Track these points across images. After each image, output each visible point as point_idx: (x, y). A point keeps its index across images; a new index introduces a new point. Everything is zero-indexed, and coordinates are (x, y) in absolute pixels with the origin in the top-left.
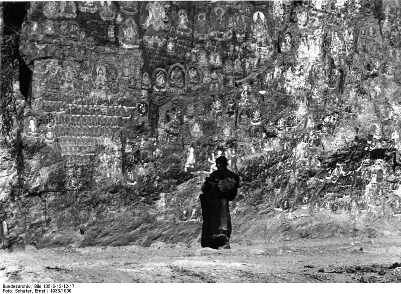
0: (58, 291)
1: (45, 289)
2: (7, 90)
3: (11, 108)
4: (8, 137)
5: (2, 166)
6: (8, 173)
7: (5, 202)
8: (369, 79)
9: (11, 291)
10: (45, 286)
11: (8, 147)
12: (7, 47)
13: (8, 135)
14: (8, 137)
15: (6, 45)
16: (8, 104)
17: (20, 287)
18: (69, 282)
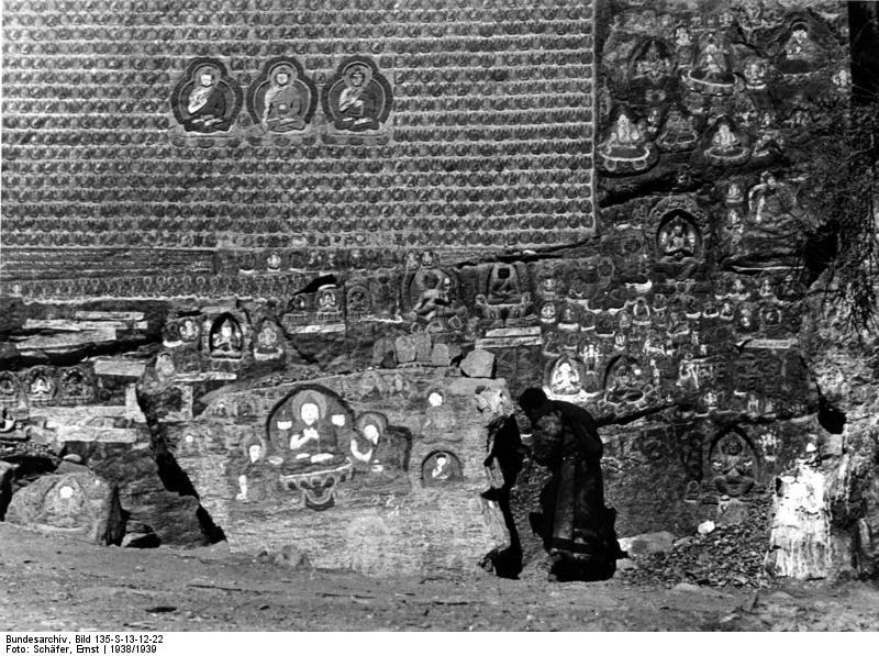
0: (127, 649)
1: (100, 645)
2: (861, 229)
3: (871, 266)
4: (865, 333)
5: (853, 395)
6: (866, 411)
7: (862, 477)
8: (348, 223)
9: (23, 650)
10: (100, 639)
11: (865, 355)
12: (861, 133)
13: (866, 327)
14: (865, 333)
15: (859, 129)
16: (865, 257)
17: (43, 640)
18: (113, 630)
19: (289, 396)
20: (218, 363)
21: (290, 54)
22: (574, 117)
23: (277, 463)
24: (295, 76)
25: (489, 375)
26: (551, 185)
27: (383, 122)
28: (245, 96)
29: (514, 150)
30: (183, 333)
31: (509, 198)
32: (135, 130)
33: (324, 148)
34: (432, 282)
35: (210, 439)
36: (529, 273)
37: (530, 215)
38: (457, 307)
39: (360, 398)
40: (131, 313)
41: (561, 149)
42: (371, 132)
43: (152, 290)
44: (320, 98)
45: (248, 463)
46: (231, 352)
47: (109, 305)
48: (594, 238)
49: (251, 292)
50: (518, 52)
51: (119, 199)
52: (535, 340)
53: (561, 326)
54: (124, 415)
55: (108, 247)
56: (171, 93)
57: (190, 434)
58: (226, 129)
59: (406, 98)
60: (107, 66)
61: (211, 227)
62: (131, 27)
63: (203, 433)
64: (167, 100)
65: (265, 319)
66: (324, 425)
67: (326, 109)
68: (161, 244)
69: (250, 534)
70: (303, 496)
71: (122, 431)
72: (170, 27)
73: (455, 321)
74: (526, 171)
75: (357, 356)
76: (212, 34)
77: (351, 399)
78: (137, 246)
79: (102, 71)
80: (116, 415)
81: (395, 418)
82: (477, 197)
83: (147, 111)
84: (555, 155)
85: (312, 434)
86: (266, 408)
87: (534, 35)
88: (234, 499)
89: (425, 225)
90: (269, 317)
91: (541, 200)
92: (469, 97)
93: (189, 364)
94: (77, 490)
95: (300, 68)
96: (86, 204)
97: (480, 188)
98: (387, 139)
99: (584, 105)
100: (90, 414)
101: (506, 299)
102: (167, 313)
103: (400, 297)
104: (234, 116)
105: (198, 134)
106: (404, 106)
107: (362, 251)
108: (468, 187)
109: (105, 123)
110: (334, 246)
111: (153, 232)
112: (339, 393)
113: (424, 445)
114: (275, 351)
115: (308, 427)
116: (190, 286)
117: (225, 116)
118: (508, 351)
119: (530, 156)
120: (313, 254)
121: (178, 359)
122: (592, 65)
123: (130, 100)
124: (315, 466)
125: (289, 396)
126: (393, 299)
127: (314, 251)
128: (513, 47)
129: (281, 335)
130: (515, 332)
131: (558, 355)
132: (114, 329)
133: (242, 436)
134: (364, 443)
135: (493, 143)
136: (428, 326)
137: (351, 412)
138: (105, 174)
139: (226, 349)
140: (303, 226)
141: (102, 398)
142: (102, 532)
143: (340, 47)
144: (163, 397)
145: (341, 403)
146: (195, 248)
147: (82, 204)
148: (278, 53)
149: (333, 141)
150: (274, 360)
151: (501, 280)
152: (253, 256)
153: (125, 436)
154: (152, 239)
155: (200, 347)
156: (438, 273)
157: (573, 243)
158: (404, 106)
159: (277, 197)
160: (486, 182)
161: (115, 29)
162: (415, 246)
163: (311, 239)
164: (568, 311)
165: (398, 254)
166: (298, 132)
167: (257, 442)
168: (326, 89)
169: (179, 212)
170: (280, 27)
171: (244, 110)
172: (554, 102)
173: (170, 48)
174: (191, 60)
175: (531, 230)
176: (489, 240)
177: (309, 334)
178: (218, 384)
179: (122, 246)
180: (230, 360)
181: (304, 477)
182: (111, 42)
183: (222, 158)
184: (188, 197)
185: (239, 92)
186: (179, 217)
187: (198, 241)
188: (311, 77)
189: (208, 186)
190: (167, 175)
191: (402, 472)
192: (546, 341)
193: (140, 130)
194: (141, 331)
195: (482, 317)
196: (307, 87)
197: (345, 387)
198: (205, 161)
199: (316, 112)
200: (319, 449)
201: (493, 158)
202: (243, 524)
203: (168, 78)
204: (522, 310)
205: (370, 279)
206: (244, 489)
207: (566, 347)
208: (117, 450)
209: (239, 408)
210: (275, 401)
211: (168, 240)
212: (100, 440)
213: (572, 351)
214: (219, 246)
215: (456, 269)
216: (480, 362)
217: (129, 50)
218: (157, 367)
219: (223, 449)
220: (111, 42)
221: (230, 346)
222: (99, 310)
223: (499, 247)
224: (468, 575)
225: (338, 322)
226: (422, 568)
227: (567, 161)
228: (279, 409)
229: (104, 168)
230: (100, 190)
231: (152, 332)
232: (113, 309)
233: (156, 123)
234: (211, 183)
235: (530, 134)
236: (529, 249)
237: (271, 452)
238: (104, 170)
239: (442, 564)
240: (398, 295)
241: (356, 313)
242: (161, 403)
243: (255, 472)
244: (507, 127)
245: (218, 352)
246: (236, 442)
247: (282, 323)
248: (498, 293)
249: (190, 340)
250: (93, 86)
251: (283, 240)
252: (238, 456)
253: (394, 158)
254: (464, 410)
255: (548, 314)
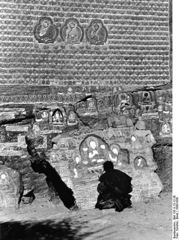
19: (85, 139)
20: (55, 127)
21: (74, 17)
22: (164, 44)
23: (86, 163)
24: (76, 25)
25: (144, 129)
26: (157, 66)
27: (105, 42)
28: (59, 32)
29: (146, 54)
30: (42, 116)
31: (145, 69)
32: (21, 42)
33: (87, 50)
34: (123, 97)
35: (61, 156)
36: (155, 95)
37: (151, 75)
38: (132, 106)
39: (109, 139)
40: (20, 109)
41: (160, 54)
42: (101, 45)
43: (28, 100)
44: (85, 33)
45: (76, 164)
46: (60, 123)
47: (12, 106)
48: (170, 83)
49: (62, 101)
50: (146, 21)
51: (16, 67)
52: (157, 117)
53: (164, 112)
54: (17, 146)
55: (12, 84)
56: (33, 29)
57: (53, 154)
58: (53, 43)
59: (112, 35)
60: (10, 18)
61: (48, 77)
62: (18, 4)
63: (58, 154)
64: (32, 31)
65: (70, 110)
66: (98, 148)
67: (87, 38)
68: (31, 84)
69: (81, 190)
70: (97, 175)
71: (17, 151)
72: (32, 5)
73: (132, 111)
74: (150, 61)
75: (102, 123)
76: (48, 8)
77: (106, 139)
78: (22, 84)
79: (8, 19)
80: (14, 146)
81: (123, 146)
82: (134, 69)
83: (25, 35)
84: (158, 56)
85: (96, 152)
86: (78, 143)
87: (151, 16)
88: (73, 177)
89: (119, 78)
90: (72, 110)
91: (154, 70)
92: (132, 35)
93: (45, 127)
94: (7, 175)
95: (78, 23)
96: (4, 69)
97: (136, 66)
98: (106, 49)
99: (167, 40)
100: (5, 146)
101: (148, 103)
102: (33, 108)
103: (114, 103)
104: (55, 38)
105: (43, 44)
106: (112, 37)
107: (99, 87)
108: (132, 65)
109: (10, 39)
110: (90, 85)
111: (28, 79)
112: (102, 137)
113: (133, 155)
114: (75, 122)
115: (94, 150)
116: (41, 99)
117: (53, 38)
118: (149, 120)
119: (151, 56)
120: (83, 87)
121: (41, 125)
122: (168, 27)
123: (19, 31)
124: (99, 164)
125: (85, 139)
126: (112, 103)
127: (83, 86)
128: (145, 19)
129: (76, 116)
130: (150, 114)
131: (163, 122)
132: (14, 115)
133: (72, 154)
134: (114, 155)
135: (140, 51)
136: (124, 113)
137: (107, 144)
138: (10, 58)
139: (57, 121)
140: (80, 78)
141: (8, 140)
142: (19, 191)
143: (91, 16)
144: (36, 140)
145: (103, 141)
146: (42, 85)
147: (2, 68)
148: (70, 17)
149: (90, 48)
150: (75, 125)
151: (145, 97)
152: (63, 88)
153: (18, 153)
154: (28, 82)
155: (48, 121)
156: (125, 95)
157: (163, 84)
158: (112, 37)
159: (71, 67)
160: (138, 64)
161: (12, 4)
162: (116, 85)
163: (83, 82)
164: (166, 107)
165: (110, 88)
166: (78, 45)
167: (77, 156)
168: (87, 30)
169: (37, 72)
170: (71, 7)
171: (59, 36)
172: (158, 38)
173: (33, 12)
174: (40, 17)
175: (151, 80)
176: (138, 83)
177: (86, 116)
178: (56, 135)
179: (17, 84)
180: (59, 126)
181: (96, 168)
182: (11, 9)
183: (52, 53)
184: (40, 66)
185: (57, 30)
186: (37, 74)
187: (43, 82)
188: (82, 26)
189: (47, 63)
190: (33, 58)
191: (127, 164)
192: (160, 117)
193: (23, 42)
194: (24, 115)
195: (140, 109)
196: (80, 29)
197: (104, 135)
198: (46, 54)
199: (84, 38)
200: (99, 157)
201: (140, 56)
202: (78, 187)
203: (32, 23)
204: (153, 107)
205: (105, 97)
206: (76, 173)
207: (166, 119)
208: (16, 159)
209: (69, 144)
210: (81, 141)
211: (33, 82)
212: (9, 155)
213: (167, 120)
214: (51, 84)
215: (131, 93)
216: (141, 124)
217: (17, 12)
218: (33, 129)
219: (66, 159)
220: (11, 9)
221: (59, 121)
222: (8, 108)
223: (142, 86)
224: (156, 200)
225: (95, 111)
226: (141, 199)
227: (161, 58)
228: (83, 144)
229: (10, 55)
230: (9, 64)
231: (28, 115)
232: (14, 107)
233: (28, 40)
234: (47, 62)
235: (151, 49)
236: (151, 86)
237: (83, 160)
238: (10, 56)
239: (147, 197)
240: (113, 102)
241: (101, 108)
242: (36, 142)
243: (79, 166)
244: (144, 46)
245: (55, 123)
246: (70, 156)
247: (77, 112)
248: (145, 101)
249: (45, 119)
250: (5, 25)
251: (73, 82)
252: (71, 161)
253: (109, 55)
254: (143, 142)
255: (160, 108)
